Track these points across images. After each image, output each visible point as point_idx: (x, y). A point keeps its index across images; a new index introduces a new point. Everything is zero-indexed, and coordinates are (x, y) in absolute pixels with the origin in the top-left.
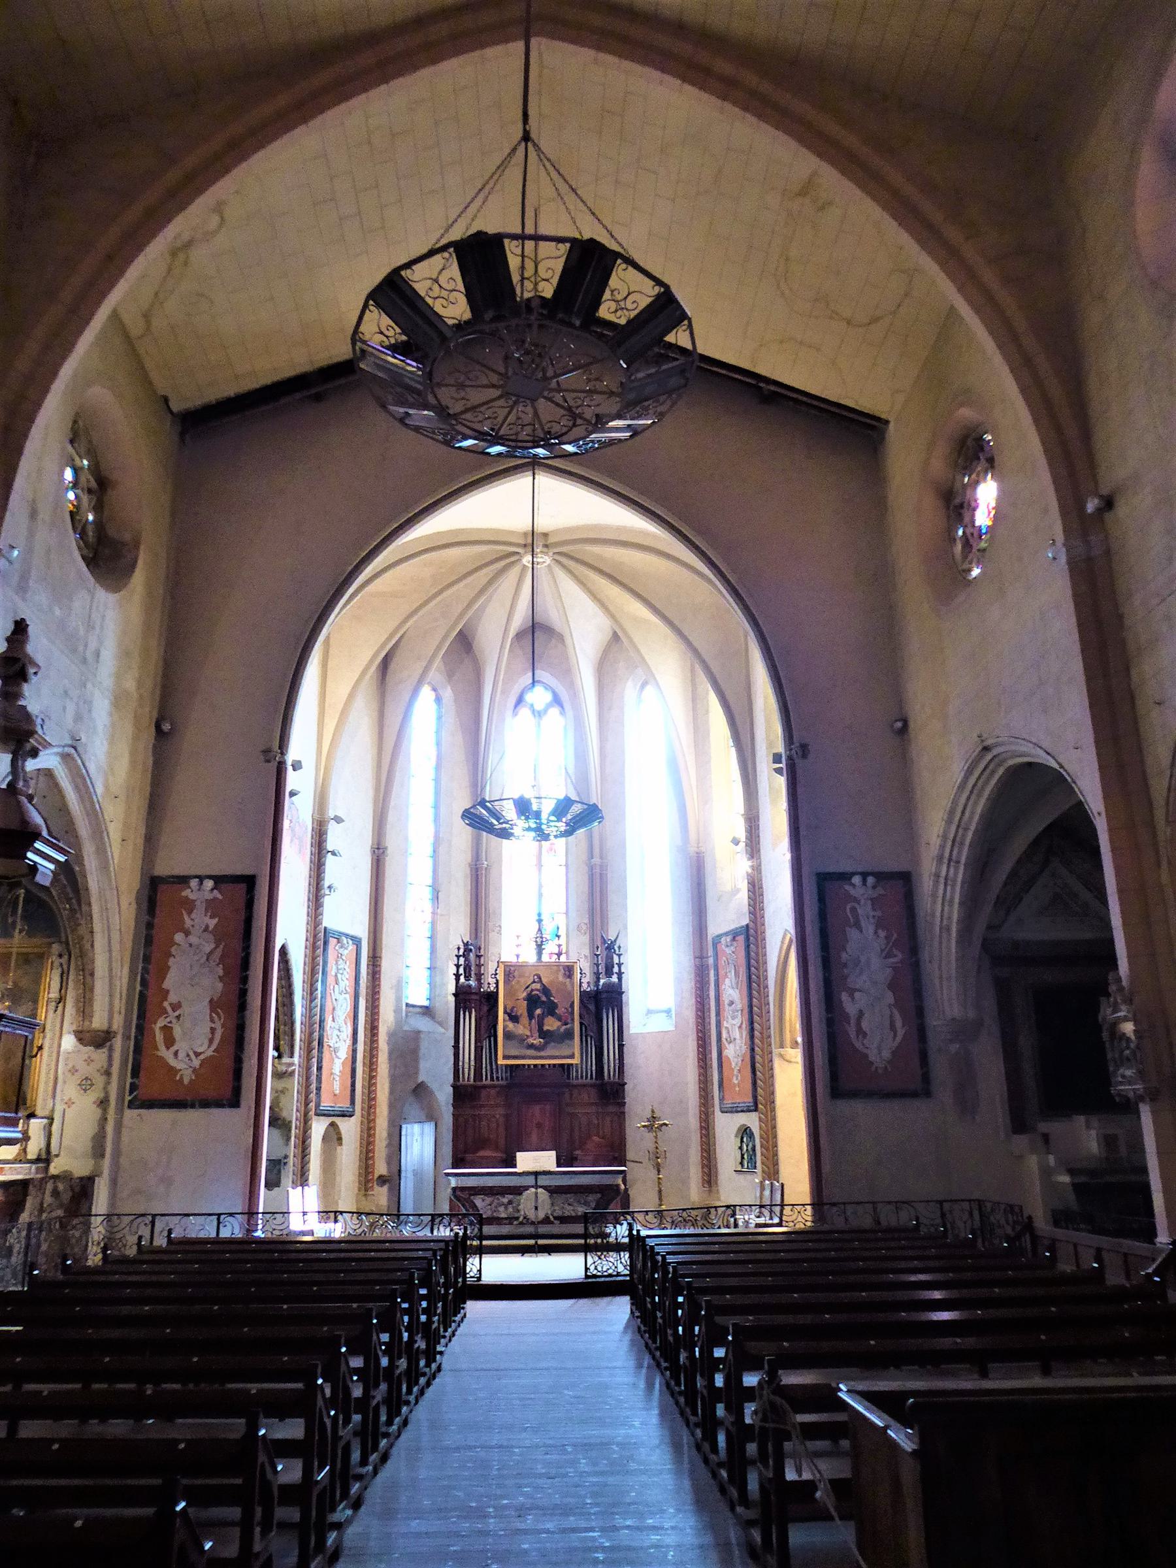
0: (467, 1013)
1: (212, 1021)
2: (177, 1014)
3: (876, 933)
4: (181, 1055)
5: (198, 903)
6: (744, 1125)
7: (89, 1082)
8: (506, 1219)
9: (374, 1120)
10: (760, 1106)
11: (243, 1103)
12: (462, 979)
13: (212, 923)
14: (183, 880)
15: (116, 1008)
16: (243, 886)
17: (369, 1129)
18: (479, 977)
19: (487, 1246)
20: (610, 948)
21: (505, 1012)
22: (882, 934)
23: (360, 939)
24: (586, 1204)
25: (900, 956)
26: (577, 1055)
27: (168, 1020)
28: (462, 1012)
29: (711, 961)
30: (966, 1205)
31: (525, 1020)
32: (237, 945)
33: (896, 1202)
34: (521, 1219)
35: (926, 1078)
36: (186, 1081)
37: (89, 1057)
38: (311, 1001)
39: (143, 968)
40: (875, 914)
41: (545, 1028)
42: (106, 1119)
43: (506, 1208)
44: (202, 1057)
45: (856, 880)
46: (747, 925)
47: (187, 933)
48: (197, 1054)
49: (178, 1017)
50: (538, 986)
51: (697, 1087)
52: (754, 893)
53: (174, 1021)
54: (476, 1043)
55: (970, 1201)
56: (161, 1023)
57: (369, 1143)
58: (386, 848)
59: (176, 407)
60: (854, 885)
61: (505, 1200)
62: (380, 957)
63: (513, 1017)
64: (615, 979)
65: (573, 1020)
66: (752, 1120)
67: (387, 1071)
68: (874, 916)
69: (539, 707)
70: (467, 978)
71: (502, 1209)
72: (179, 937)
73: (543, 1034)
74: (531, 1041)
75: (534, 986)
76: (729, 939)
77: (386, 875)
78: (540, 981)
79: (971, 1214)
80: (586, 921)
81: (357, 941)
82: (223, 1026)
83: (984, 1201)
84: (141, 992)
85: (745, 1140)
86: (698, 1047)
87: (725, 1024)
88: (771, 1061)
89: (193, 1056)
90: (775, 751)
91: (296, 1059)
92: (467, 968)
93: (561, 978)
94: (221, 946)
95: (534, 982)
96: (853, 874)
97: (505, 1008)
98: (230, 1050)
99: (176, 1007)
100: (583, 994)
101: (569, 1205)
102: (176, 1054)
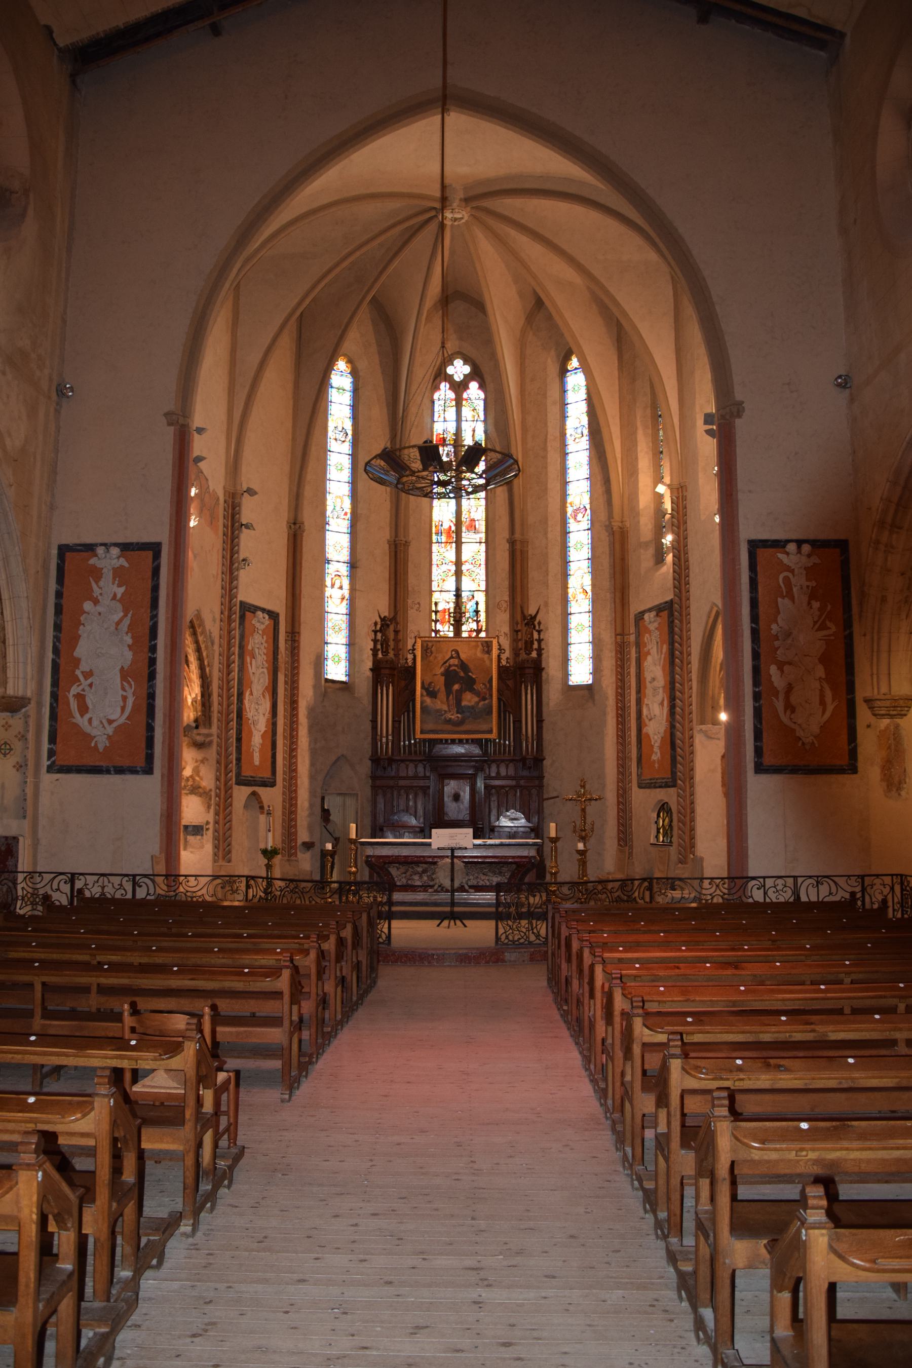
0: (385, 688)
1: (123, 689)
2: (89, 681)
3: (809, 603)
4: (95, 723)
5: (105, 570)
6: (662, 800)
7: (8, 747)
8: (421, 886)
9: (296, 791)
10: (679, 782)
11: (155, 771)
12: (380, 655)
13: (120, 591)
14: (90, 548)
15: (29, 677)
16: (150, 554)
17: (291, 799)
18: (397, 651)
19: (396, 912)
20: (531, 622)
21: (423, 687)
22: (816, 605)
23: (278, 614)
24: (500, 873)
25: (834, 629)
26: (495, 730)
27: (81, 687)
28: (379, 687)
29: (632, 638)
30: (888, 880)
31: (442, 695)
32: (146, 613)
33: (818, 877)
34: (436, 887)
35: (853, 754)
36: (101, 747)
37: (7, 723)
38: (228, 674)
39: (55, 637)
40: (808, 583)
41: (463, 704)
42: (26, 782)
43: (421, 877)
44: (115, 725)
45: (791, 547)
46: (672, 600)
47: (96, 602)
48: (110, 722)
49: (91, 685)
50: (456, 661)
51: (615, 763)
52: (680, 567)
53: (87, 688)
54: (393, 718)
55: (892, 875)
56: (75, 690)
57: (291, 813)
58: (303, 523)
59: (63, 41)
60: (788, 554)
61: (420, 869)
62: (299, 633)
63: (430, 692)
64: (534, 654)
65: (491, 695)
66: (669, 795)
67: (307, 744)
68: (808, 587)
69: (458, 378)
70: (385, 653)
71: (416, 877)
72: (88, 606)
73: (460, 709)
74: (449, 716)
75: (452, 661)
76: (653, 614)
77: (304, 550)
78: (458, 657)
79: (892, 889)
80: (507, 598)
81: (273, 616)
82: (134, 694)
83: (906, 876)
84: (53, 661)
85: (661, 814)
86: (618, 724)
87: (646, 701)
88: (692, 737)
89: (106, 724)
90: (709, 411)
91: (214, 730)
92: (385, 642)
93: (479, 654)
94: (130, 615)
95: (452, 657)
96: (788, 541)
97: (423, 683)
98: (143, 718)
99: (88, 675)
100: (502, 670)
101: (484, 874)
102: (90, 720)
